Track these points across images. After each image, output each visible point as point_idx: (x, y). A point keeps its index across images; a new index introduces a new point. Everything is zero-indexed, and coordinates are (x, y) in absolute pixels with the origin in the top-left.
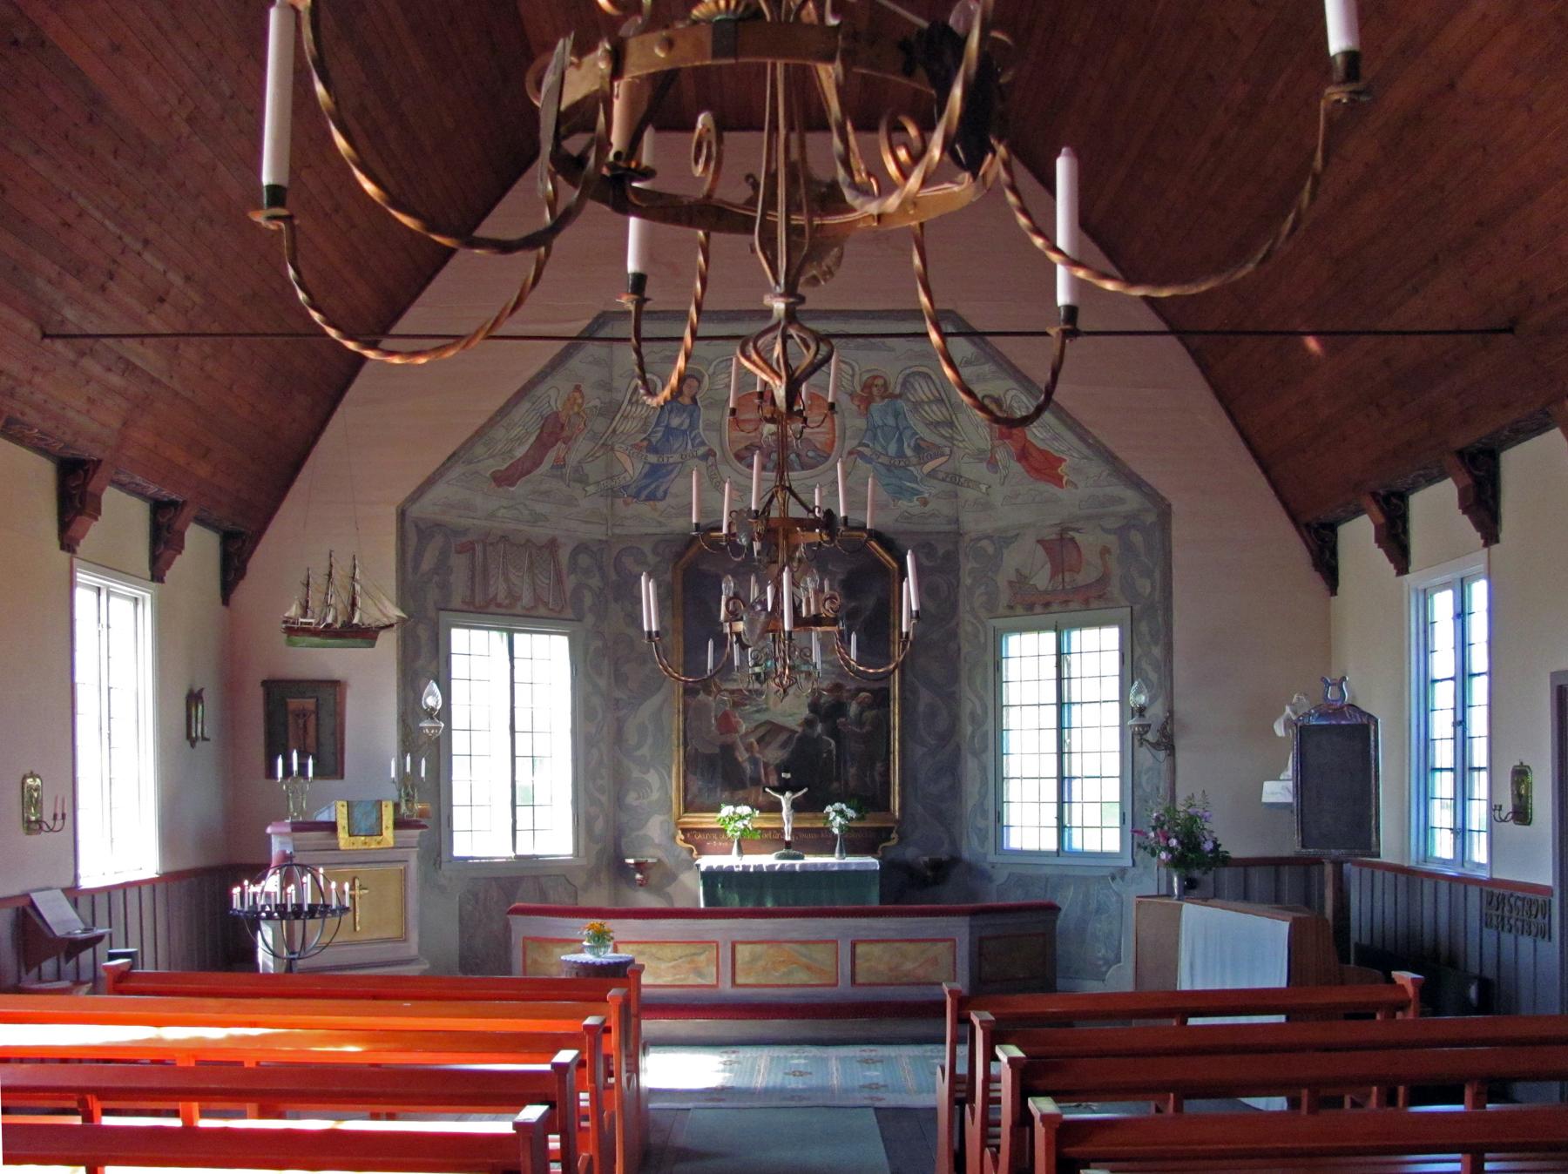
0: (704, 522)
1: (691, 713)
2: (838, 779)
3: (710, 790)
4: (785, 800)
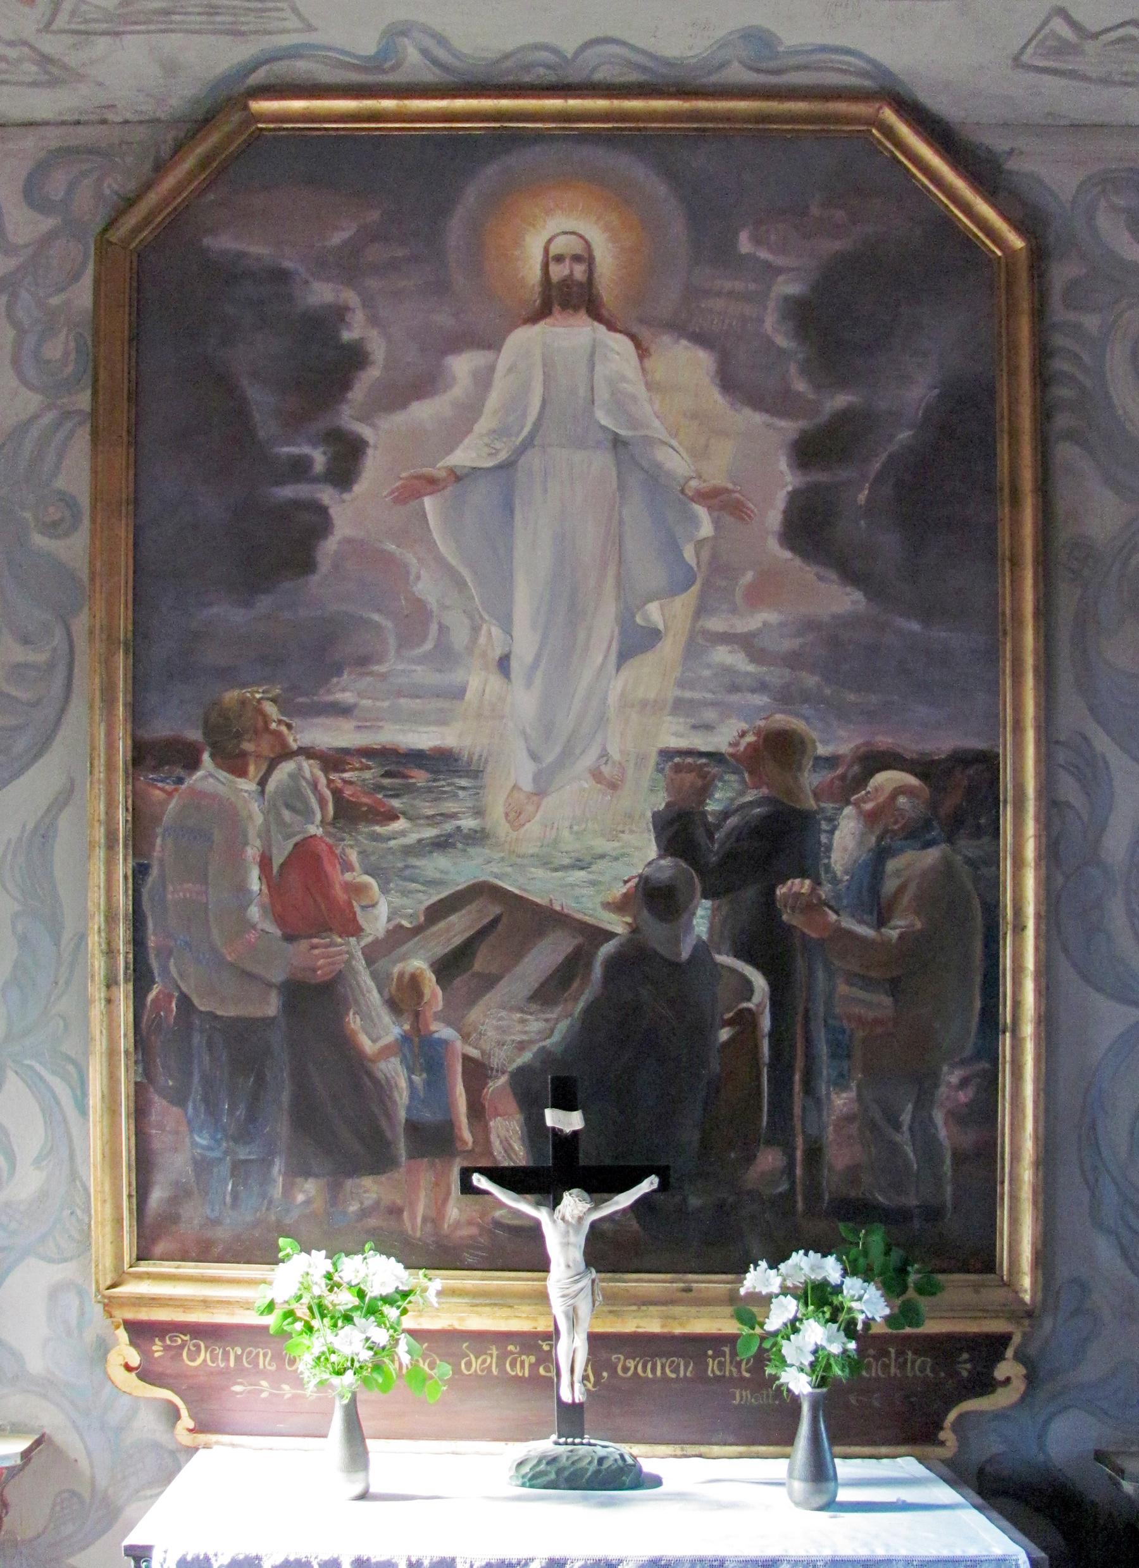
0: (414, 504)
1: (161, 848)
2: (781, 1135)
3: (239, 1169)
4: (565, 1224)
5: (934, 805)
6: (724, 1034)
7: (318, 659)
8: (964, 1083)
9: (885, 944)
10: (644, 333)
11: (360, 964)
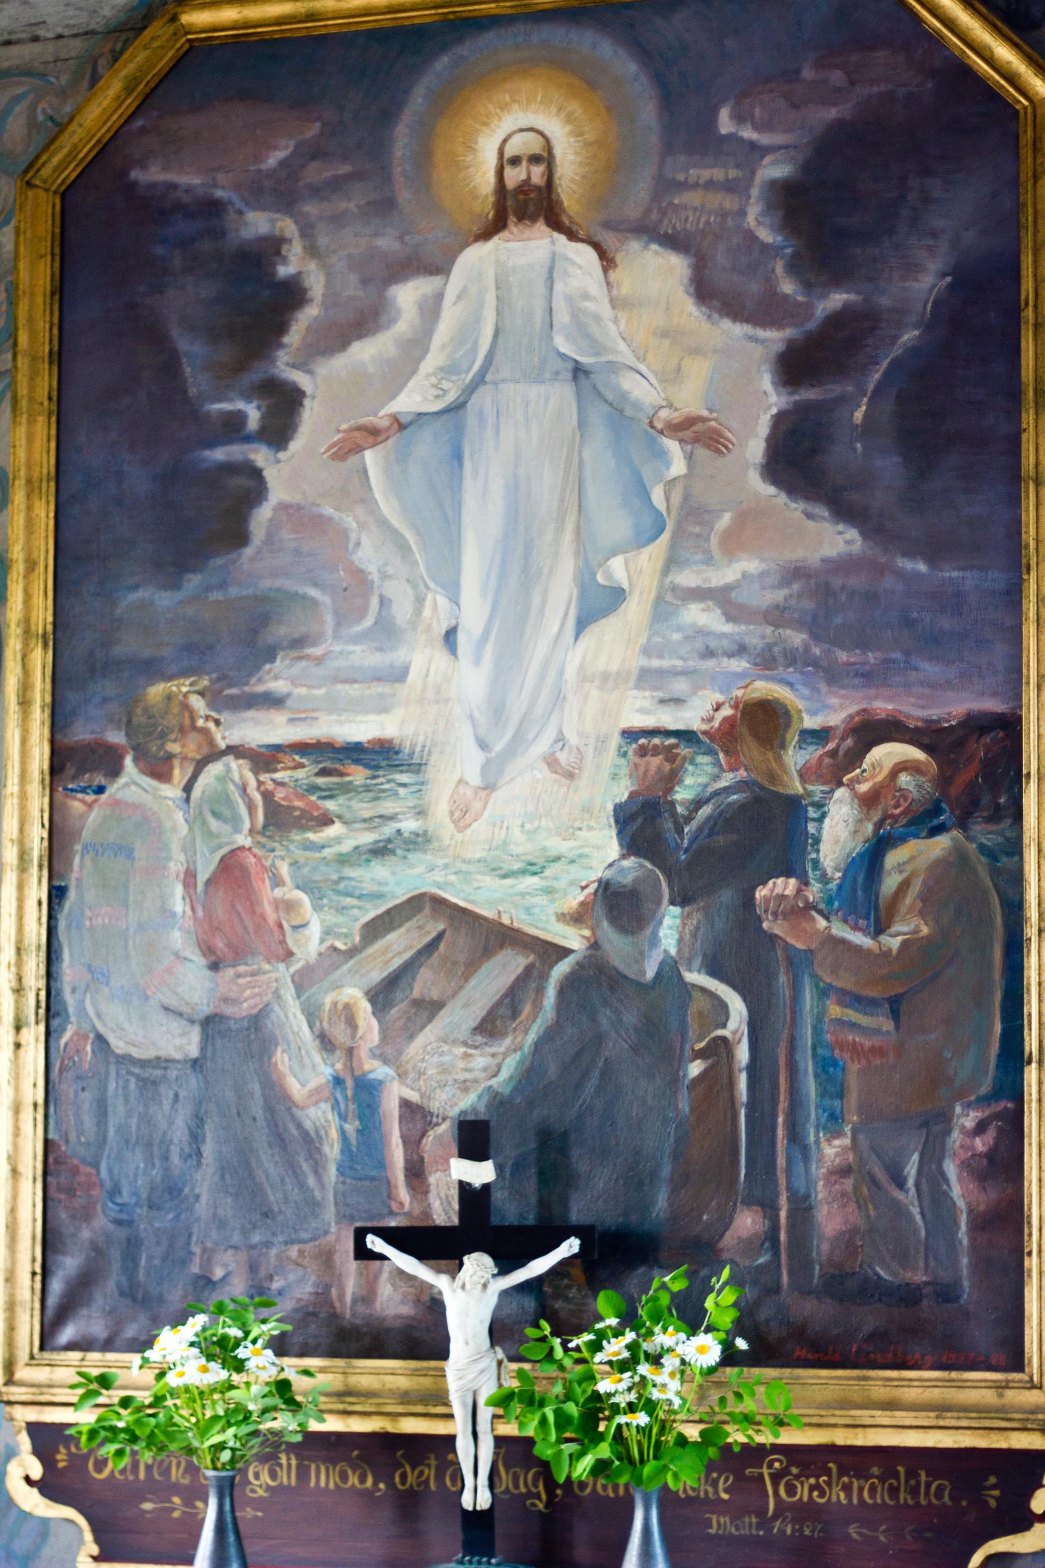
5: (944, 781)
6: (695, 1068)
7: (242, 648)
8: (980, 1128)
9: (885, 954)
10: (608, 239)
11: (289, 994)
